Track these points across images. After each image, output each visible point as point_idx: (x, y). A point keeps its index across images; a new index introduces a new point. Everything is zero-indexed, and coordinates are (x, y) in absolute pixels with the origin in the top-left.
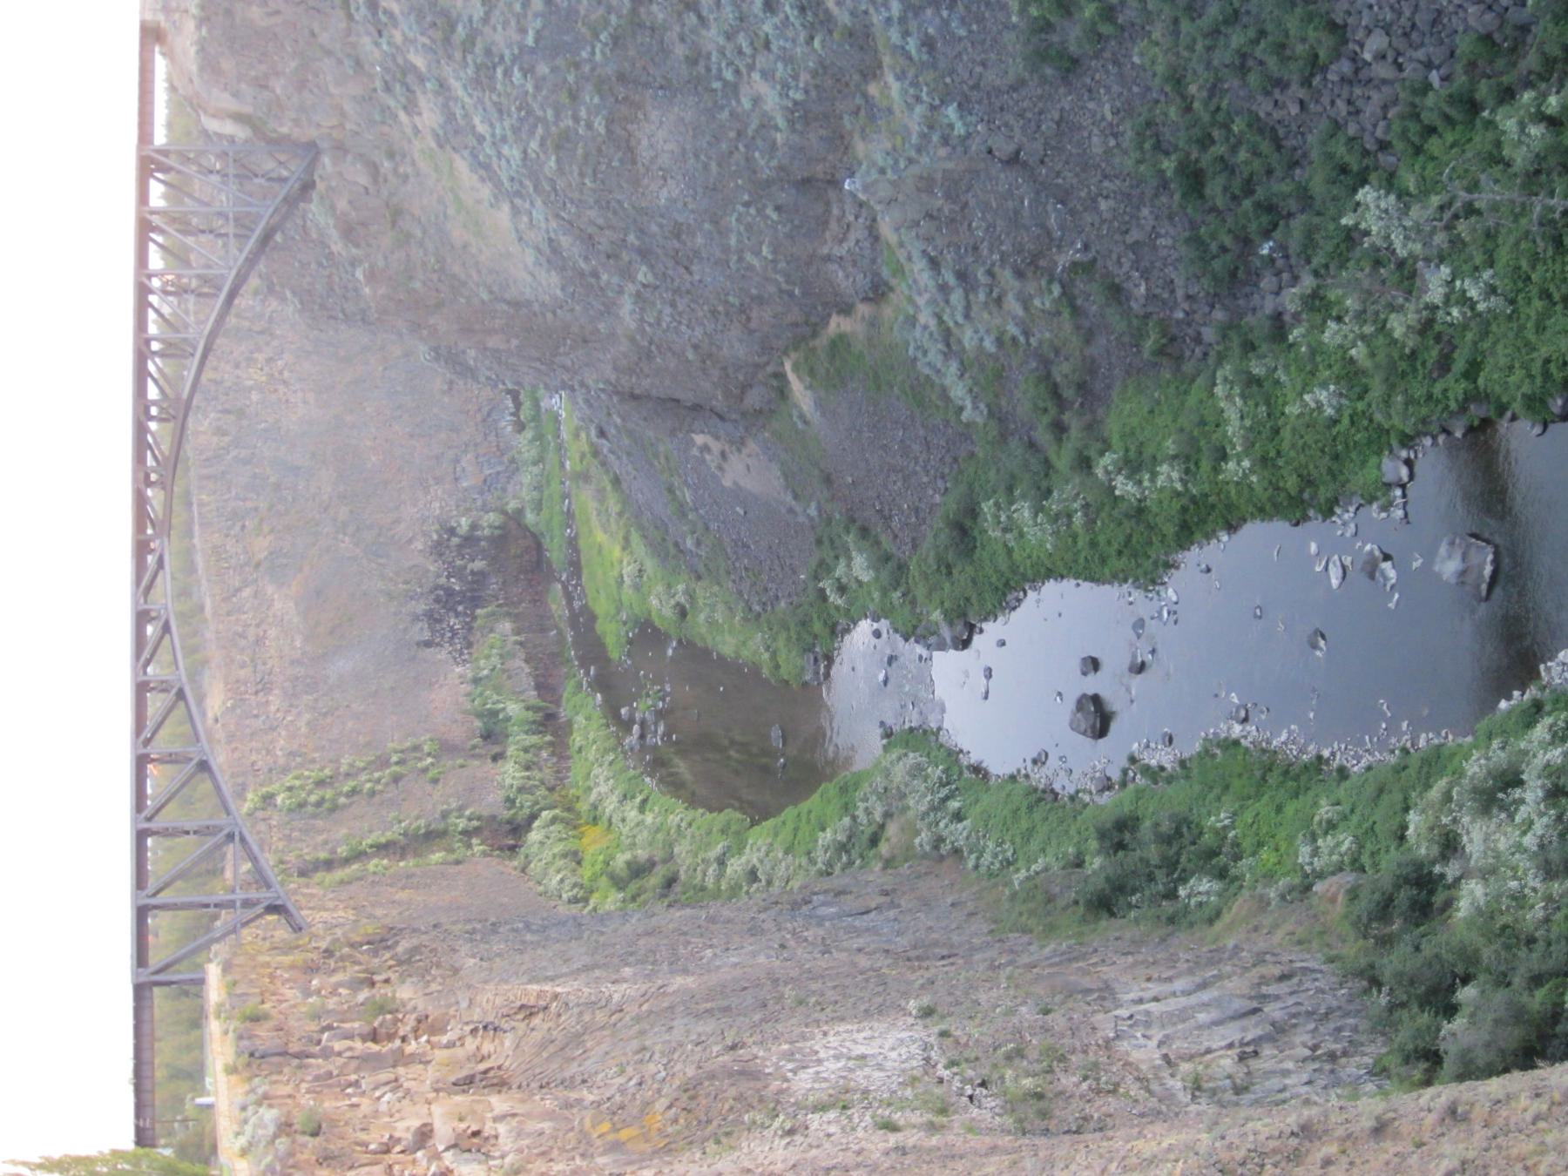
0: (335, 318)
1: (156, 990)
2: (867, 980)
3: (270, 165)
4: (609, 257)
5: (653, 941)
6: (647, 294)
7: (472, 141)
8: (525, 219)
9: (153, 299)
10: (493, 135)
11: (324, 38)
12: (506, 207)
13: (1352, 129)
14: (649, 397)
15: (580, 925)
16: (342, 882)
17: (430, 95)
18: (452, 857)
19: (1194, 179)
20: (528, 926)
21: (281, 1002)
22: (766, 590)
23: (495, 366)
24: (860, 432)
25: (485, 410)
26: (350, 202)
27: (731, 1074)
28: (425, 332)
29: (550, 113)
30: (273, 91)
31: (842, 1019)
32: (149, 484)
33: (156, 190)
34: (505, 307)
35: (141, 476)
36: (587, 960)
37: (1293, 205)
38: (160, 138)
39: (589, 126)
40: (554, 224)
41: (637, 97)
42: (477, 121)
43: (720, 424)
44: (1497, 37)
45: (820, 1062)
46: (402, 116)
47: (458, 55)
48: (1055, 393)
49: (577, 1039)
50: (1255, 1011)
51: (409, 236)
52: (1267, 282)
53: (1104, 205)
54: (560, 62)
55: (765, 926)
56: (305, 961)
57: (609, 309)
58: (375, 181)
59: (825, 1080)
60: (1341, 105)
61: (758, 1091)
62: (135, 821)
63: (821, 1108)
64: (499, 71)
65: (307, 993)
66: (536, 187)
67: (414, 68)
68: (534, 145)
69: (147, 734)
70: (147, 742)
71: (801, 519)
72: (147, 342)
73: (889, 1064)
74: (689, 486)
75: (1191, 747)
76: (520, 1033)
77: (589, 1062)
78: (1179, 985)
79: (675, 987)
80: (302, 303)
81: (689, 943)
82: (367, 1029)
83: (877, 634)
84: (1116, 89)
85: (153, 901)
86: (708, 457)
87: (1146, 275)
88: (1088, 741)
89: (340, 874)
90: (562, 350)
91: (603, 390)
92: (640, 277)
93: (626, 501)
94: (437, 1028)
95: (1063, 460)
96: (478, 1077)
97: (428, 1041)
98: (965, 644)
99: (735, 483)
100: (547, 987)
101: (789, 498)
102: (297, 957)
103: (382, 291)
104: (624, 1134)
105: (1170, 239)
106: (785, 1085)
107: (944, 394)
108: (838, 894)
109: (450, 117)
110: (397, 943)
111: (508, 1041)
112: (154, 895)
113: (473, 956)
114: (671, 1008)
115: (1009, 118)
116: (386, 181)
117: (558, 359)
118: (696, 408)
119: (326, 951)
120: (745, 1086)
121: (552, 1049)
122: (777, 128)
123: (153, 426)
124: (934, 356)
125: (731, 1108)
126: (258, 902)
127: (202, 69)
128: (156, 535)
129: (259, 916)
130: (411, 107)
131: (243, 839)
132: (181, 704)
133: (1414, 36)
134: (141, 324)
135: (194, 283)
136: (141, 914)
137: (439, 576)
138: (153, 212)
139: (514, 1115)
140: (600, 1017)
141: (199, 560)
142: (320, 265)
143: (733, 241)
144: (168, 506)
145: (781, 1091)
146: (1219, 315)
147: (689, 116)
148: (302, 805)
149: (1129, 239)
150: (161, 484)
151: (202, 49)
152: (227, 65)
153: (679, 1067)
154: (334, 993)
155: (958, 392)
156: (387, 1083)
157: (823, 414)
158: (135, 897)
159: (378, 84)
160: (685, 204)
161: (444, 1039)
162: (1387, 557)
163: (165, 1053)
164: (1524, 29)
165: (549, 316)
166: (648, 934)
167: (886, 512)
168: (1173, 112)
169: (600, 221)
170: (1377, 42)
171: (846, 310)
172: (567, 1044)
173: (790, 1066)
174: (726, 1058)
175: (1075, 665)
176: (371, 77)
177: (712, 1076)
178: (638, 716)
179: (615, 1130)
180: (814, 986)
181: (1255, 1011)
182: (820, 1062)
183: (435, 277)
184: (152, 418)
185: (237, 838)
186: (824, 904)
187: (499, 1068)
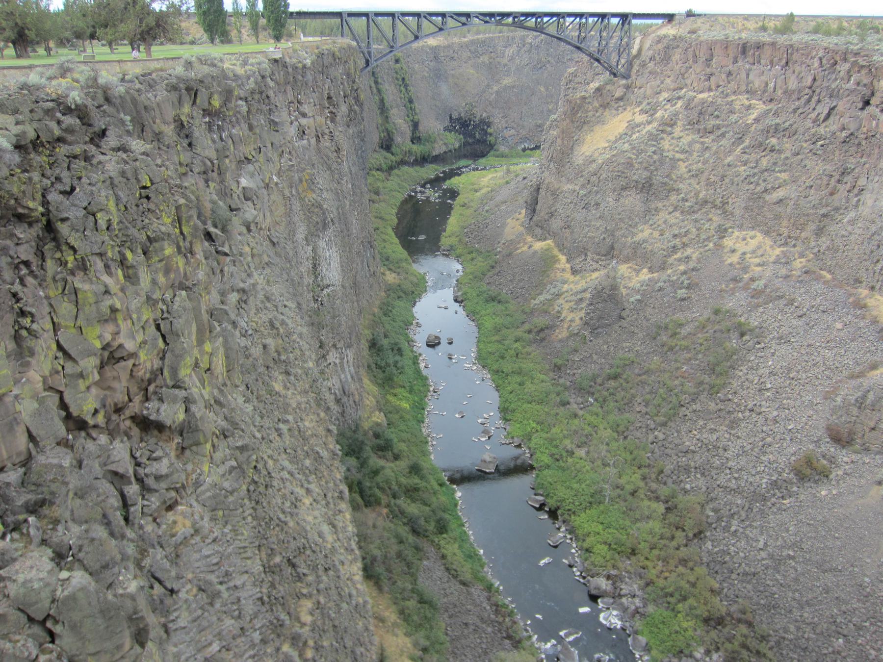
6: (575, 194)
7: (630, 133)
9: (578, 19)
11: (668, 81)
12: (607, 145)
13: (631, 428)
16: (371, 87)
19: (615, 377)
27: (324, 220)
29: (640, 160)
33: (615, 21)
37: (605, 408)
38: (634, 22)
39: (635, 174)
40: (600, 162)
42: (637, 134)
44: (662, 475)
47: (661, 128)
48: (542, 330)
50: (344, 393)
51: (597, 111)
52: (580, 400)
53: (605, 347)
54: (658, 163)
57: (569, 181)
60: (639, 425)
63: (314, 250)
64: (655, 143)
65: (341, 74)
67: (656, 113)
70: (425, 17)
72: (563, 17)
75: (425, 372)
78: (352, 368)
82: (332, 95)
84: (645, 351)
85: (370, 20)
87: (581, 360)
88: (425, 339)
89: (373, 85)
93: (500, 187)
94: (333, 120)
95: (519, 333)
98: (456, 301)
101: (503, 241)
102: (352, 71)
103: (578, 102)
104: (304, 183)
105: (593, 369)
107: (541, 294)
109: (638, 125)
111: (328, 144)
114: (340, 201)
115: (635, 316)
118: (534, 211)
120: (320, 226)
122: (632, 238)
123: (534, 20)
124: (553, 291)
127: (658, 36)
128: (497, 21)
130: (643, 112)
133: (663, 448)
134: (570, 15)
136: (366, 15)
140: (336, 176)
143: (593, 223)
144: (507, 25)
146: (568, 383)
147: (637, 208)
148: (397, 73)
149: (594, 355)
151: (665, 36)
152: (660, 46)
154: (342, 83)
155: (541, 298)
159: (650, 100)
161: (328, 122)
162: (489, 438)
164: (665, 484)
168: (637, 371)
170: (661, 436)
171: (568, 261)
175: (449, 336)
177: (324, 213)
179: (306, 180)
181: (344, 393)
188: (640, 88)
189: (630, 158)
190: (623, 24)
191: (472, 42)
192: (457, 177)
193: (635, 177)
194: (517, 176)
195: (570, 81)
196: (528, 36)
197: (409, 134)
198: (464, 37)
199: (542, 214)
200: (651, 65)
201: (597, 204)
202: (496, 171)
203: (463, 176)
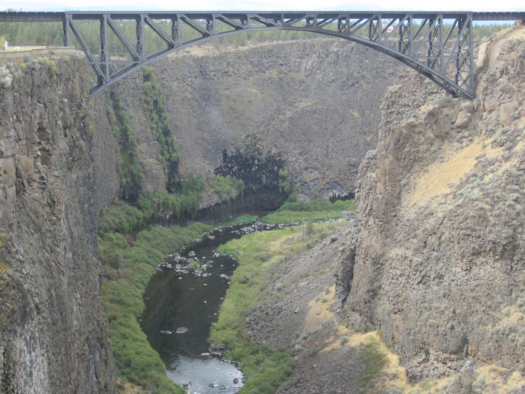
0: (388, 109)
1: (61, 23)
2: (65, 377)
3: (464, 75)
4: (425, 243)
5: (84, 268)
7: (480, 174)
8: (443, 201)
9: (397, 21)
10: (484, 184)
12: (448, 191)
14: (353, 264)
15: (92, 231)
17: (502, 153)
18: (120, 168)
20: (91, 205)
21: (57, 84)
22: (257, 324)
23: (368, 187)
24: (340, 370)
25: (341, 183)
26: (447, 115)
27: (25, 307)
28: (384, 152)
29: (497, 212)
30: (500, 77)
31: (49, 364)
32: (308, 20)
33: (449, 22)
34: (398, 192)
35: (312, 16)
36: (76, 234)
39: (490, 232)
40: (440, 215)
41: (506, 256)
42: (491, 176)
43: (341, 300)
45: (30, 352)
46: (490, 140)
49: (38, 230)
51: (432, 144)
55: (91, 324)
56: (76, 95)
58: (458, 127)
59: (20, 356)
61: (16, 321)
62: (144, 13)
64: (516, 187)
66: (459, 206)
68: (481, 205)
69: (188, 19)
70: (183, 19)
71: (293, 341)
72: (377, 18)
73: (27, 388)
74: (308, 284)
76: (42, 201)
77: (26, 235)
79: (62, 279)
80: (396, 92)
81: (83, 286)
83: (235, 381)
86: (324, 293)
90: (377, 220)
91: (357, 241)
92: (415, 259)
94: (45, 161)
96: (20, 180)
97: (38, 156)
99: (311, 307)
100: (63, 215)
101: (304, 335)
102: (78, 92)
106: (18, 335)
108: (106, 362)
109: (491, 163)
110: (84, 140)
112: (71, 25)
113: (77, 178)
114: (53, 277)
116: (458, 132)
117: (371, 218)
119: (81, 105)
120: (18, 316)
121: (33, 216)
122: (494, 326)
125: (8, 308)
126: (104, 72)
127: (510, 42)
129: (97, 73)
131: (135, 65)
132: (201, 36)
135: (405, 40)
137: (259, 160)
138: (439, 20)
139: (6, 197)
140: (49, 241)
141: (266, 43)
142: (415, 101)
145: (15, 332)
150: (308, 25)
153: (29, 281)
154: (61, 109)
156: (18, 136)
157: (348, 352)
158: (107, 13)
159: (506, 128)
160: (453, 280)
163: (34, 26)
165: (394, 214)
166: (87, 265)
167: (299, 385)
169: (443, 238)
172: (35, 225)
173: (28, 338)
174: (33, 305)
176: (510, 124)
177: (24, 297)
178: (189, 260)
180: (63, 349)
182: (30, 352)
183: (412, 157)
184: (340, 21)
185: (136, 62)
186: (101, 354)
187: (25, 191)
188: (491, 111)
189: (482, 209)
190: (460, 27)
191: (254, 52)
192: (235, 241)
193: (491, 237)
194: (323, 237)
195: (393, 103)
196: (333, 42)
197: (163, 178)
198: (243, 45)
199: (360, 293)
200: (504, 80)
201: (440, 277)
202: (293, 231)
203: (244, 238)
